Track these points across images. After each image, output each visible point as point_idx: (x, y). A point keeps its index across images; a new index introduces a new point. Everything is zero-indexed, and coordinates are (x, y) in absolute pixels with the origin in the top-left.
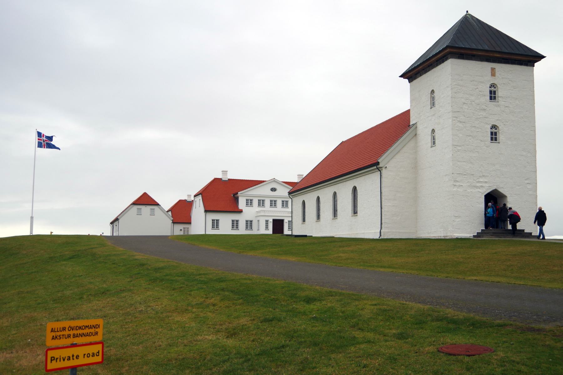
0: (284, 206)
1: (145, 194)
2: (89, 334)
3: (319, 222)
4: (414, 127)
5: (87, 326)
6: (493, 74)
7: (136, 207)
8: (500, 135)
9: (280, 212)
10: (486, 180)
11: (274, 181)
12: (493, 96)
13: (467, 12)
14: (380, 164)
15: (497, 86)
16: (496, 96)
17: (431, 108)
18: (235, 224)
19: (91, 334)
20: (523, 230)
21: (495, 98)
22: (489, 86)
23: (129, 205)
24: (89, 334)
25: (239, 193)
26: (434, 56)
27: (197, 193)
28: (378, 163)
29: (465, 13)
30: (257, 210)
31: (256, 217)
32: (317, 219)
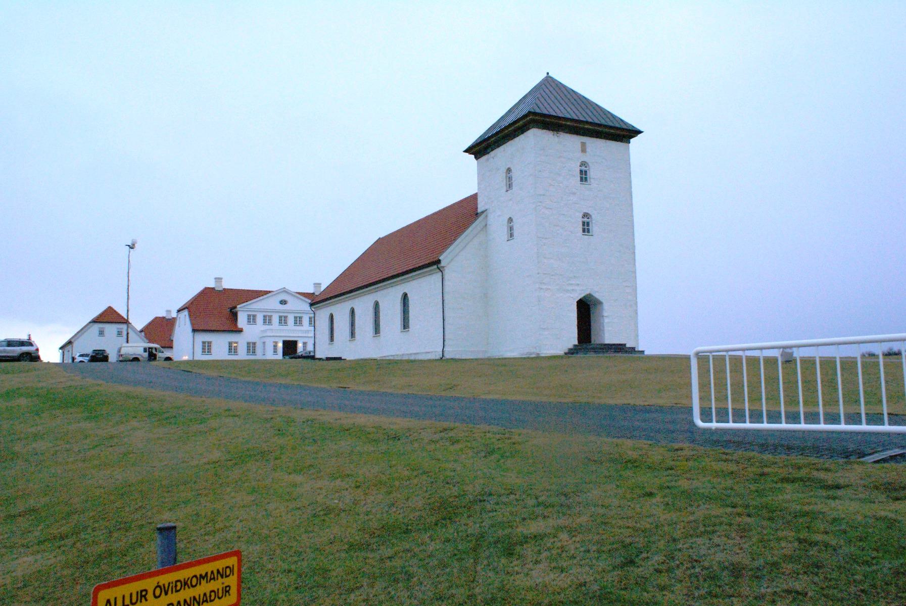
0: (297, 323)
1: (110, 308)
2: (208, 595)
3: (378, 338)
4: (483, 216)
5: (204, 575)
6: (584, 150)
7: (97, 327)
8: (594, 225)
9: (291, 332)
10: (578, 282)
11: (285, 291)
12: (584, 176)
13: (548, 73)
14: (442, 262)
15: (588, 165)
16: (588, 177)
17: (507, 191)
18: (232, 349)
19: (213, 594)
20: (625, 345)
21: (586, 179)
22: (579, 164)
23: (86, 324)
24: (208, 595)
25: (238, 306)
26: (510, 125)
27: (184, 305)
28: (439, 262)
29: (546, 75)
30: (263, 329)
31: (261, 337)
32: (374, 332)
